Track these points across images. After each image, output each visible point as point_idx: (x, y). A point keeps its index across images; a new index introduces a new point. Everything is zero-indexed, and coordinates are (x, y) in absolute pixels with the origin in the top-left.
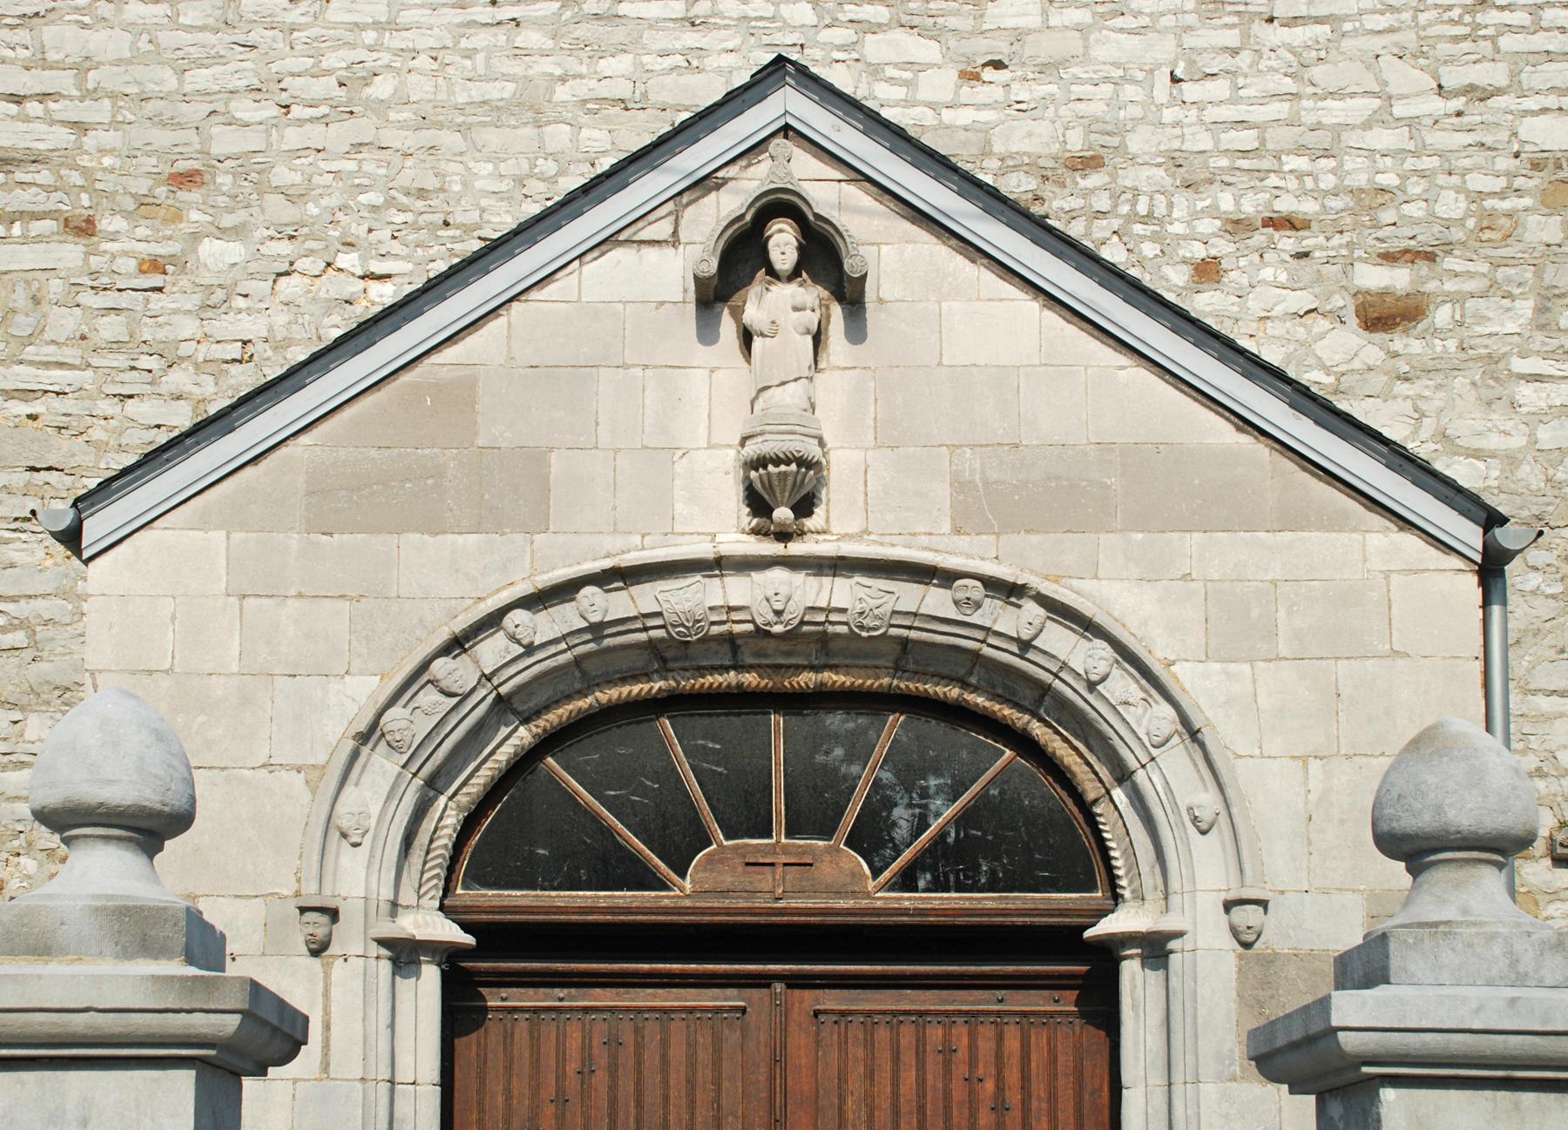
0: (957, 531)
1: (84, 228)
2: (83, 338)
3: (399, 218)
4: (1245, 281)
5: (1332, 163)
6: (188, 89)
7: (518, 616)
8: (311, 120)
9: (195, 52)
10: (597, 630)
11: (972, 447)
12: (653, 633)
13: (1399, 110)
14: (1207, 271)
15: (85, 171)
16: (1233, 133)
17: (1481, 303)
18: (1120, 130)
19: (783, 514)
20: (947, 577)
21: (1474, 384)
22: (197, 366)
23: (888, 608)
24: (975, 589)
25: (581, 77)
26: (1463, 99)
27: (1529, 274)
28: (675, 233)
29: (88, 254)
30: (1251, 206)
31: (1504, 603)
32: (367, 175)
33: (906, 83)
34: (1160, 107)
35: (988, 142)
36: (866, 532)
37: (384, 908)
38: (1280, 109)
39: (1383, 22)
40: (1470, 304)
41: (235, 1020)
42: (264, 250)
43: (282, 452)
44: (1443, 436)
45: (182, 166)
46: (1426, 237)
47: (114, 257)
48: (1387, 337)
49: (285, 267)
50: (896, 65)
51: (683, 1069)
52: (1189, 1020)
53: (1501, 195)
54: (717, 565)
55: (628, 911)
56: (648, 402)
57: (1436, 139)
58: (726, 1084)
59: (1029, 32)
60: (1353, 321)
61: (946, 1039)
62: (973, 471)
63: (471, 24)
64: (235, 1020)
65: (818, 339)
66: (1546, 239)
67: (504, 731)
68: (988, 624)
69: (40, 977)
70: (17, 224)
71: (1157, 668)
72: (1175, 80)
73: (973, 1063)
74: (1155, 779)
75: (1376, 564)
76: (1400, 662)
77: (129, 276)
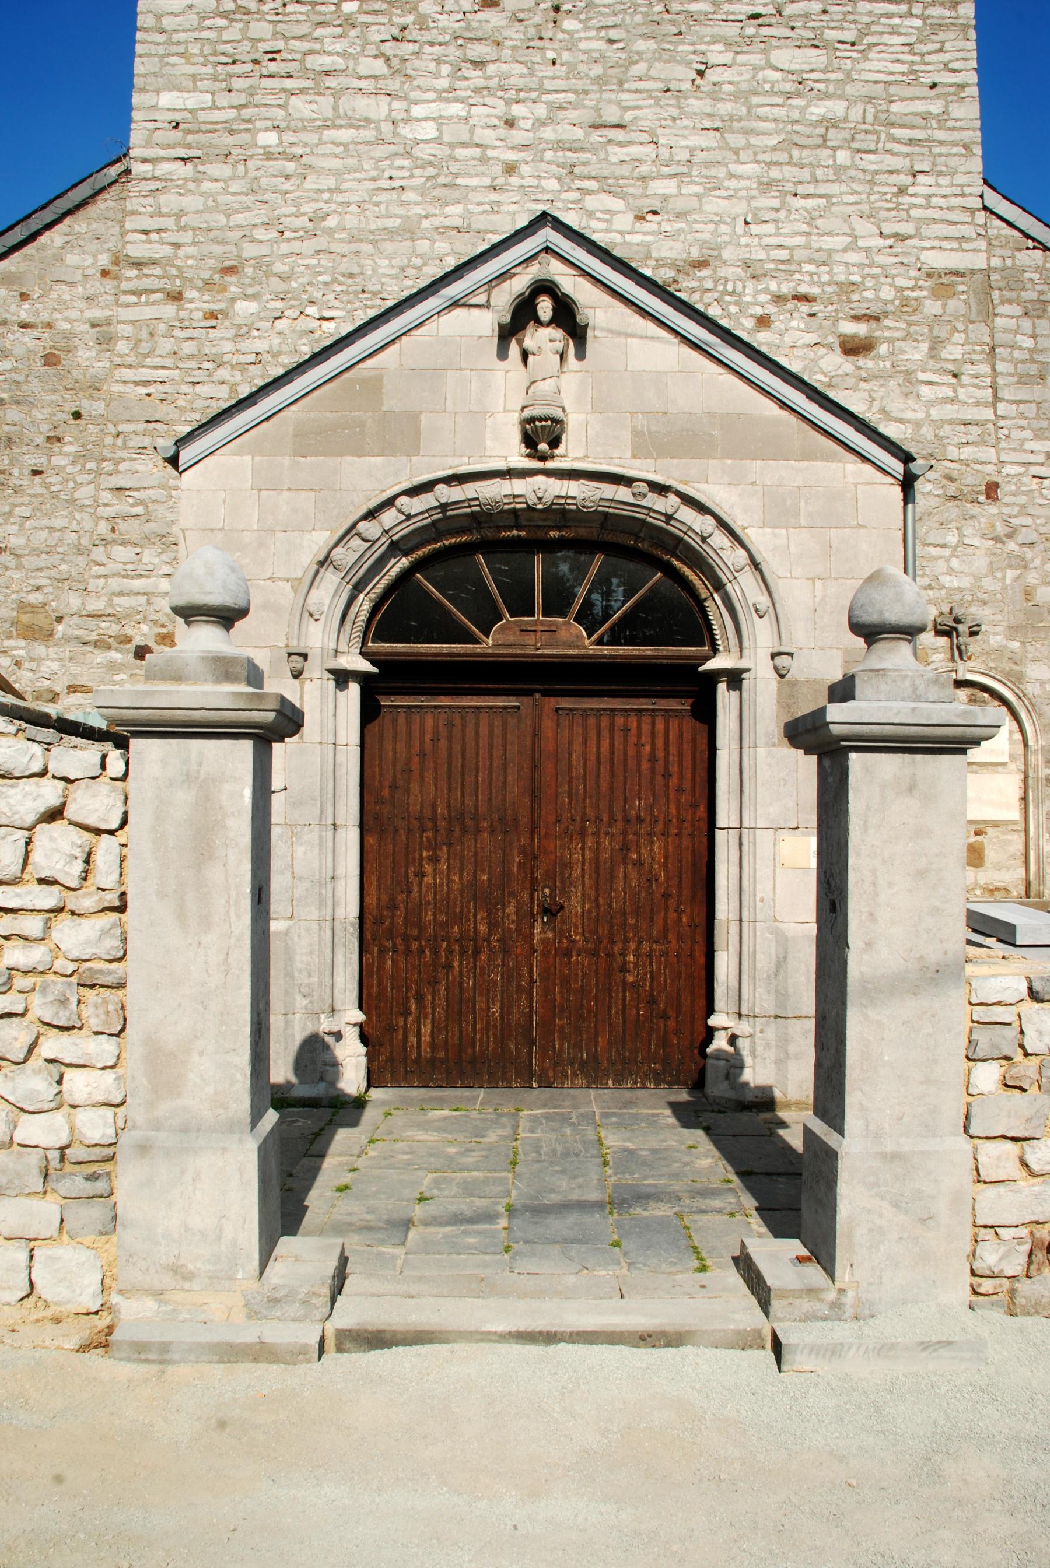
0: (634, 457)
1: (176, 297)
2: (175, 353)
3: (339, 288)
4: (783, 327)
5: (827, 269)
6: (232, 224)
7: (403, 500)
8: (295, 239)
9: (236, 206)
10: (444, 507)
11: (643, 413)
12: (474, 509)
13: (860, 243)
14: (763, 321)
15: (178, 268)
16: (776, 252)
17: (902, 344)
18: (719, 248)
19: (543, 447)
20: (627, 481)
21: (899, 384)
22: (232, 366)
23: (598, 497)
24: (644, 488)
25: (436, 215)
26: (893, 240)
27: (926, 330)
28: (488, 301)
29: (178, 310)
30: (786, 289)
31: (914, 502)
32: (322, 267)
33: (606, 221)
34: (739, 237)
35: (650, 252)
36: (587, 456)
37: (332, 653)
38: (800, 240)
39: (852, 199)
40: (897, 344)
41: (273, 715)
42: (268, 306)
43: (282, 414)
44: (883, 411)
45: (228, 263)
46: (875, 309)
47: (191, 311)
48: (855, 358)
49: (279, 314)
50: (602, 212)
51: (486, 738)
52: (752, 714)
53: (912, 289)
54: (509, 474)
55: (459, 655)
56: (473, 388)
57: (879, 259)
58: (509, 747)
59: (671, 196)
60: (838, 350)
61: (626, 724)
62: (643, 426)
63: (379, 189)
64: (273, 715)
65: (562, 356)
66: (934, 312)
67: (393, 561)
68: (650, 506)
69: (178, 692)
70: (144, 296)
71: (738, 531)
72: (747, 223)
73: (639, 736)
74: (737, 588)
75: (851, 479)
76: (862, 531)
77: (199, 321)
